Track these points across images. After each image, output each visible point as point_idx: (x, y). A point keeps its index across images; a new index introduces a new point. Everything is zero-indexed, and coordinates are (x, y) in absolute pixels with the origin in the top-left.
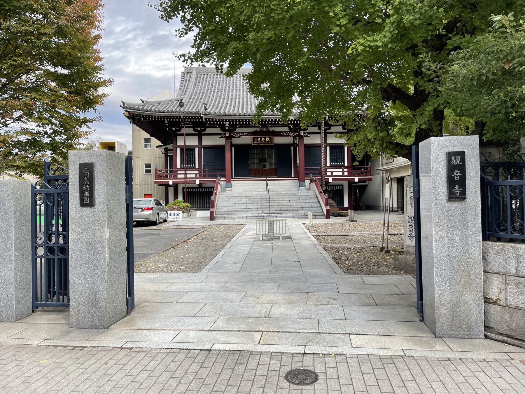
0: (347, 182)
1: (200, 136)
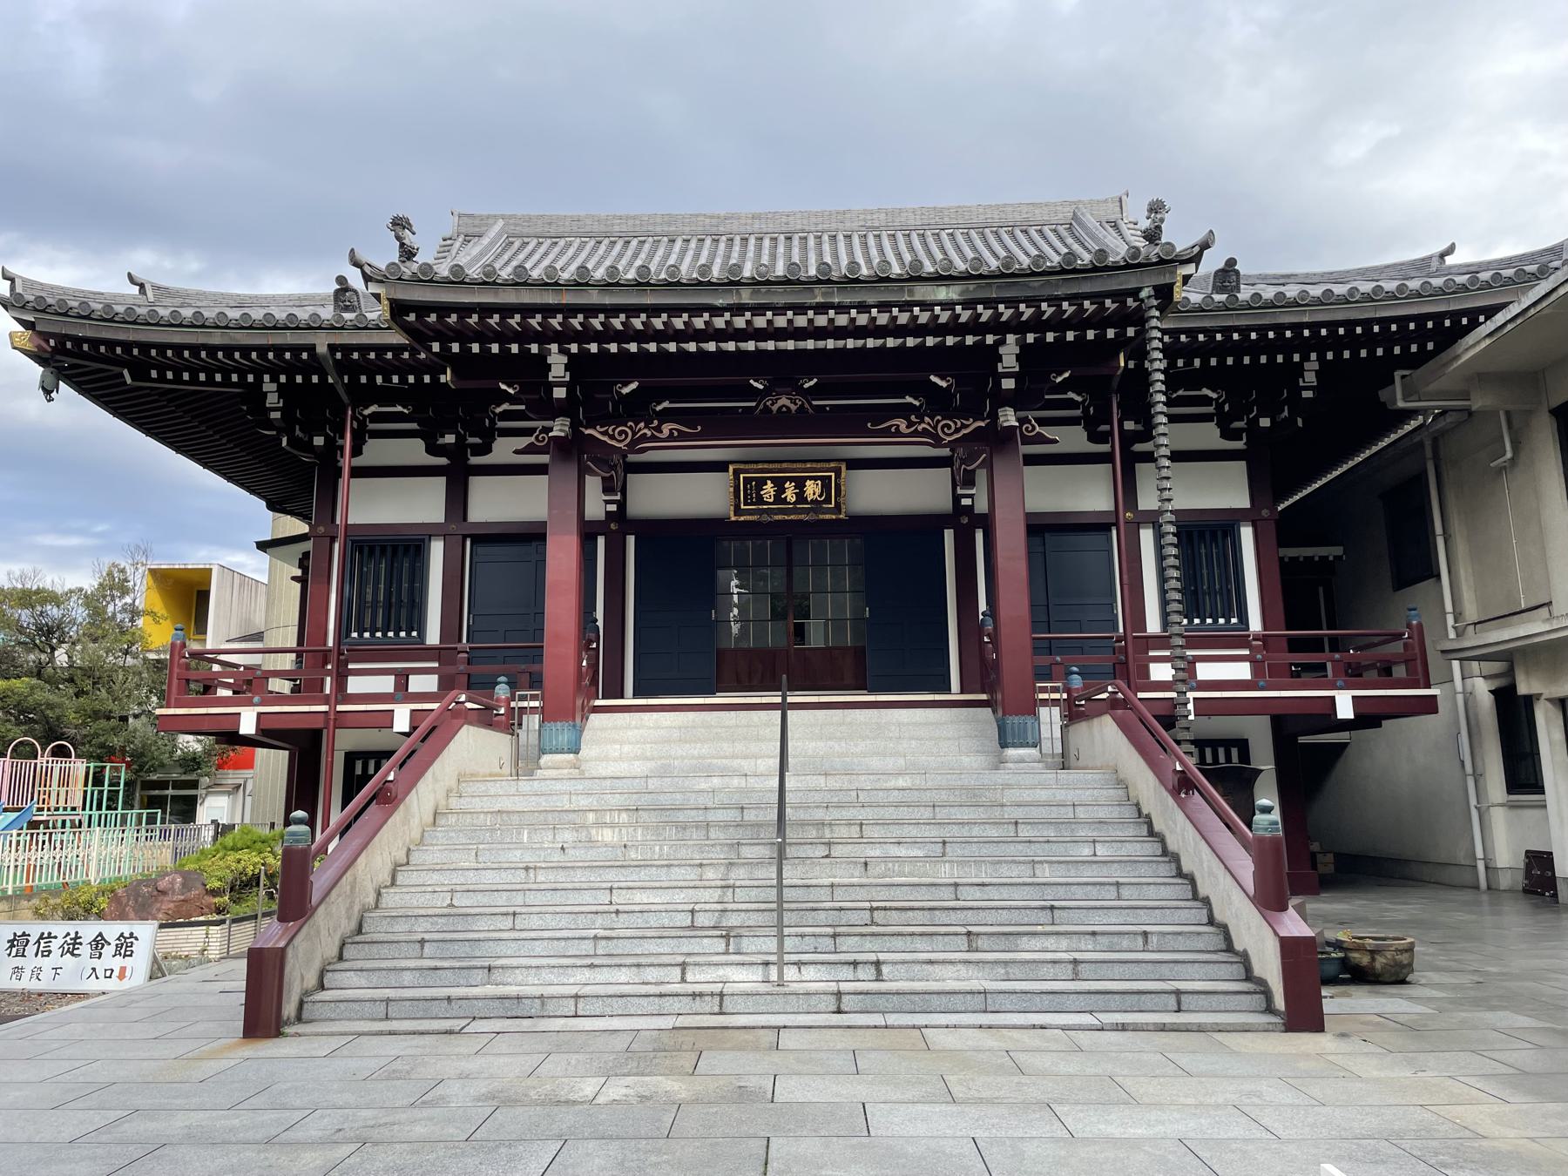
0: (1265, 721)
1: (457, 480)
